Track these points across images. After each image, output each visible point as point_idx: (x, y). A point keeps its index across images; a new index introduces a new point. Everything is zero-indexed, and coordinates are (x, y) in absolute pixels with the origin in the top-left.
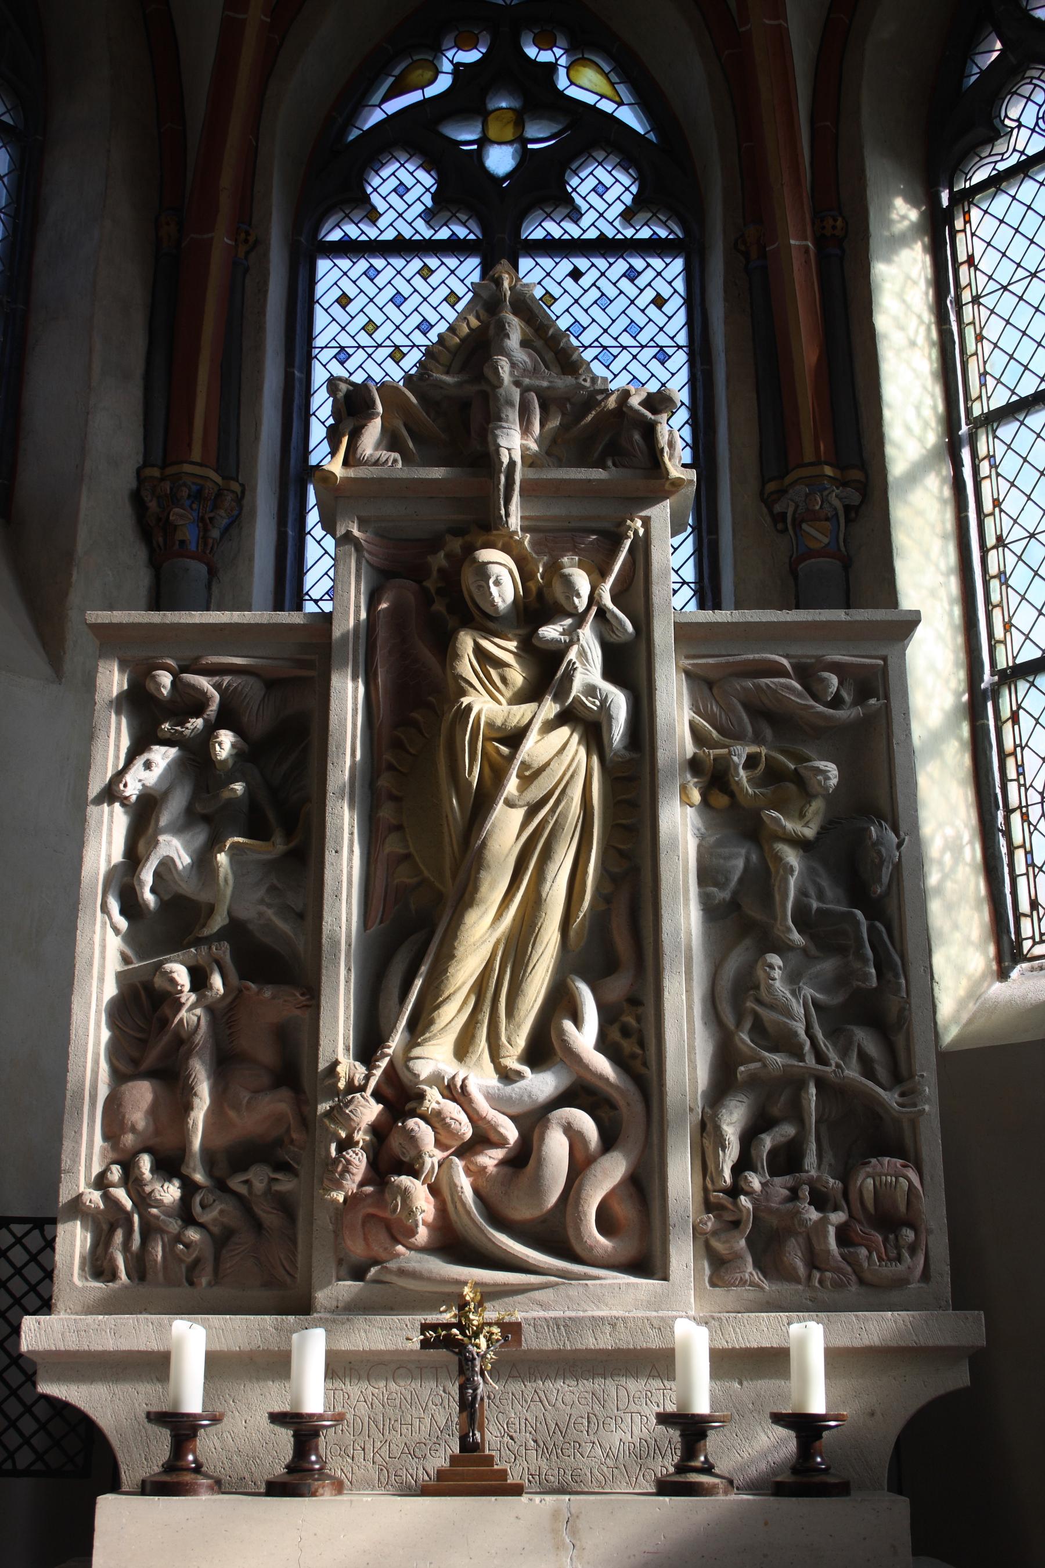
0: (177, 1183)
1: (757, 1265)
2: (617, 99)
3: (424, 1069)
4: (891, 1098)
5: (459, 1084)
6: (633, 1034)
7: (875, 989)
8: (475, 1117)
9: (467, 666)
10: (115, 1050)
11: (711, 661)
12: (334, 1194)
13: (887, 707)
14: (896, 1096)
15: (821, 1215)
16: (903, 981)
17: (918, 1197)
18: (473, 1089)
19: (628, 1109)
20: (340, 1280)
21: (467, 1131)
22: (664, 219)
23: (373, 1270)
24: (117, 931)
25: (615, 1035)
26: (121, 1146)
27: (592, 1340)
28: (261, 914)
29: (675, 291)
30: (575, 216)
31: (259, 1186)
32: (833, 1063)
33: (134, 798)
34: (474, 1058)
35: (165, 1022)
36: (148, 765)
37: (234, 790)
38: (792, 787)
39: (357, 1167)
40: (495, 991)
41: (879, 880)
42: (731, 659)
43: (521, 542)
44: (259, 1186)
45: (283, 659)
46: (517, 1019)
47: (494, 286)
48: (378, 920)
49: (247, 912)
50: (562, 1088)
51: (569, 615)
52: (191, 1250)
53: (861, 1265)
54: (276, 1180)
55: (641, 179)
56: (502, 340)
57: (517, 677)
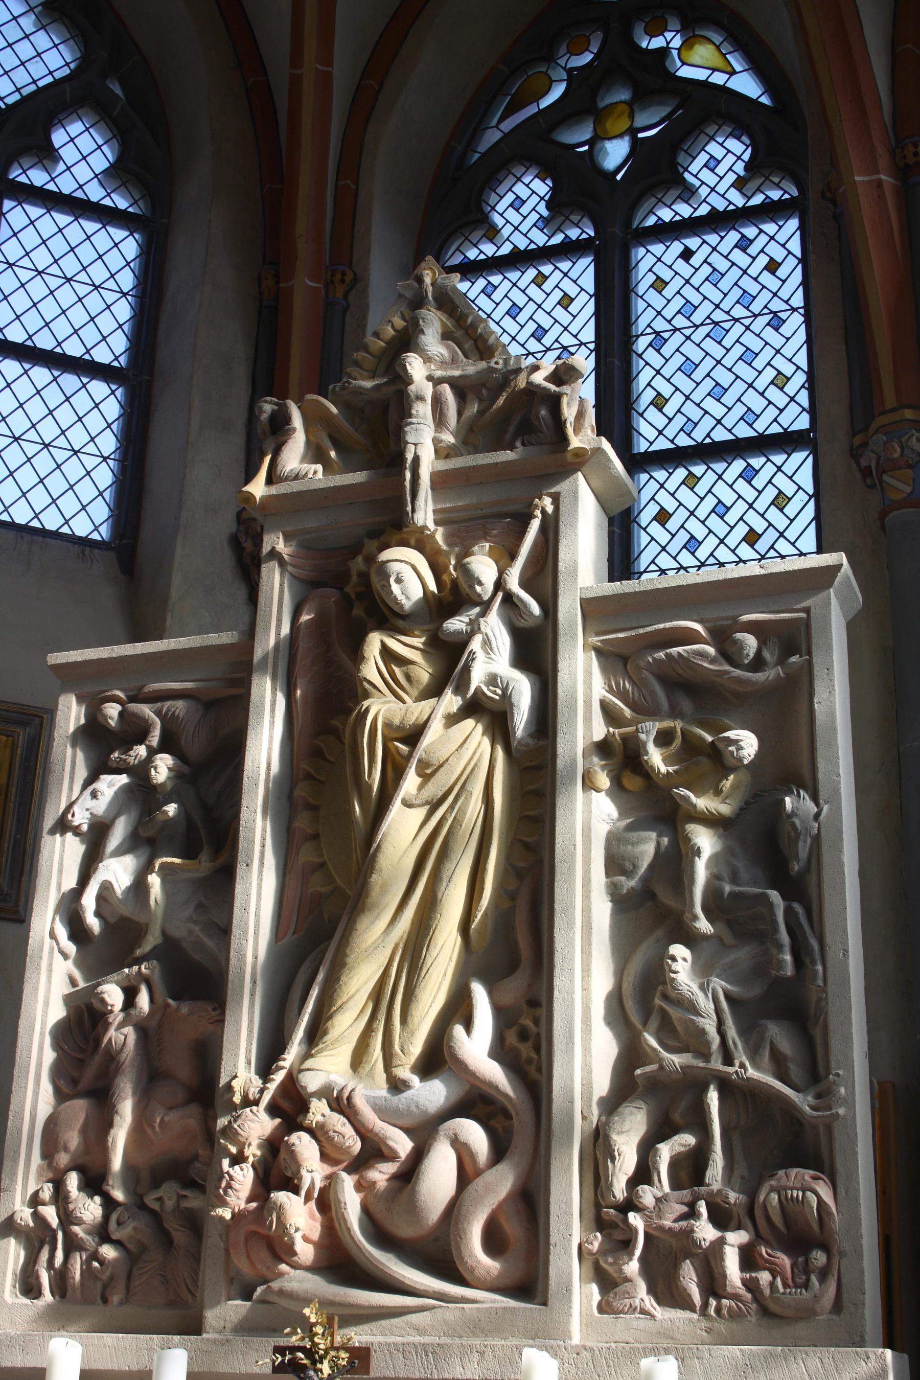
0: (97, 1199)
1: (651, 1290)
2: (729, 69)
3: (311, 1082)
4: (803, 1101)
5: (345, 1095)
6: (527, 1040)
7: (789, 978)
8: (362, 1130)
9: (371, 669)
10: (58, 1073)
11: (621, 635)
12: (219, 1211)
13: (810, 663)
14: (810, 1098)
15: (719, 1234)
16: (819, 968)
17: (830, 1214)
18: (360, 1102)
19: (519, 1117)
20: (230, 1299)
21: (356, 1145)
22: (776, 180)
23: (259, 1290)
24: (65, 956)
25: (512, 1038)
26: (55, 1164)
27: (459, 1369)
28: (190, 932)
29: (790, 252)
30: (686, 195)
31: (170, 1204)
32: (737, 1063)
33: (85, 828)
34: (367, 1068)
35: (98, 1041)
36: (94, 795)
37: (166, 812)
38: (705, 762)
39: (240, 1183)
40: (392, 998)
41: (797, 857)
42: (641, 631)
43: (432, 536)
44: (170, 1204)
45: (216, 679)
46: (411, 1026)
47: (416, 285)
48: (291, 931)
49: (179, 931)
50: (454, 1098)
51: (476, 604)
52: (104, 1268)
53: (762, 1293)
54: (185, 1196)
55: (754, 145)
56: (417, 337)
57: (424, 673)
